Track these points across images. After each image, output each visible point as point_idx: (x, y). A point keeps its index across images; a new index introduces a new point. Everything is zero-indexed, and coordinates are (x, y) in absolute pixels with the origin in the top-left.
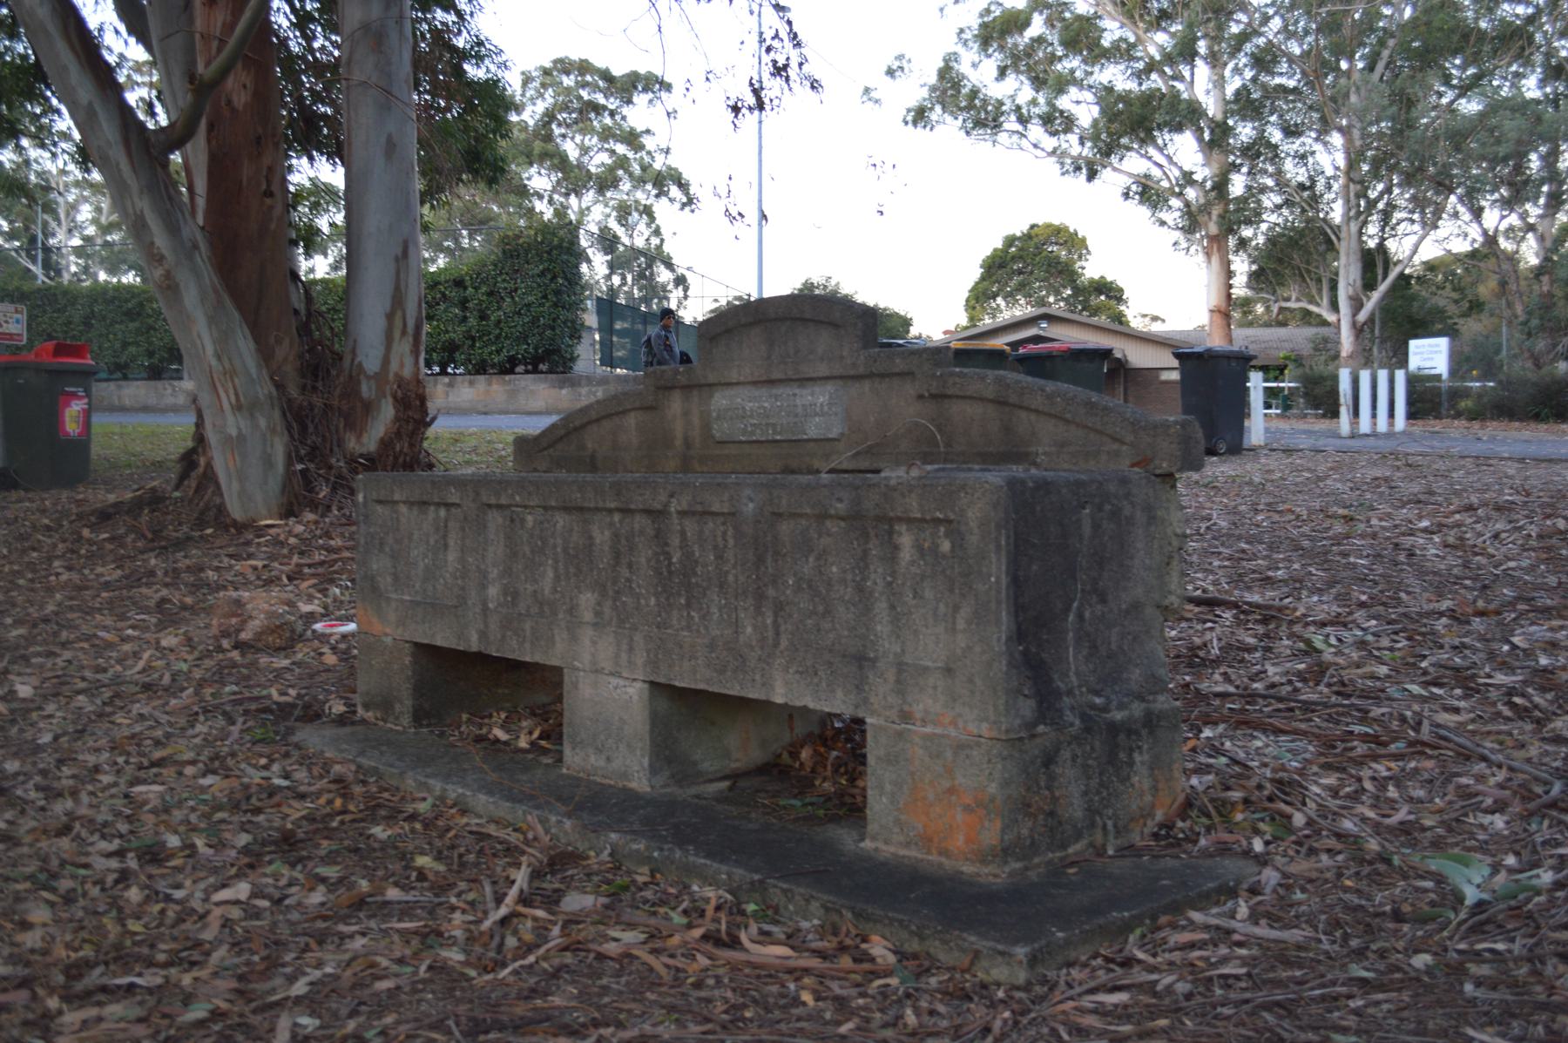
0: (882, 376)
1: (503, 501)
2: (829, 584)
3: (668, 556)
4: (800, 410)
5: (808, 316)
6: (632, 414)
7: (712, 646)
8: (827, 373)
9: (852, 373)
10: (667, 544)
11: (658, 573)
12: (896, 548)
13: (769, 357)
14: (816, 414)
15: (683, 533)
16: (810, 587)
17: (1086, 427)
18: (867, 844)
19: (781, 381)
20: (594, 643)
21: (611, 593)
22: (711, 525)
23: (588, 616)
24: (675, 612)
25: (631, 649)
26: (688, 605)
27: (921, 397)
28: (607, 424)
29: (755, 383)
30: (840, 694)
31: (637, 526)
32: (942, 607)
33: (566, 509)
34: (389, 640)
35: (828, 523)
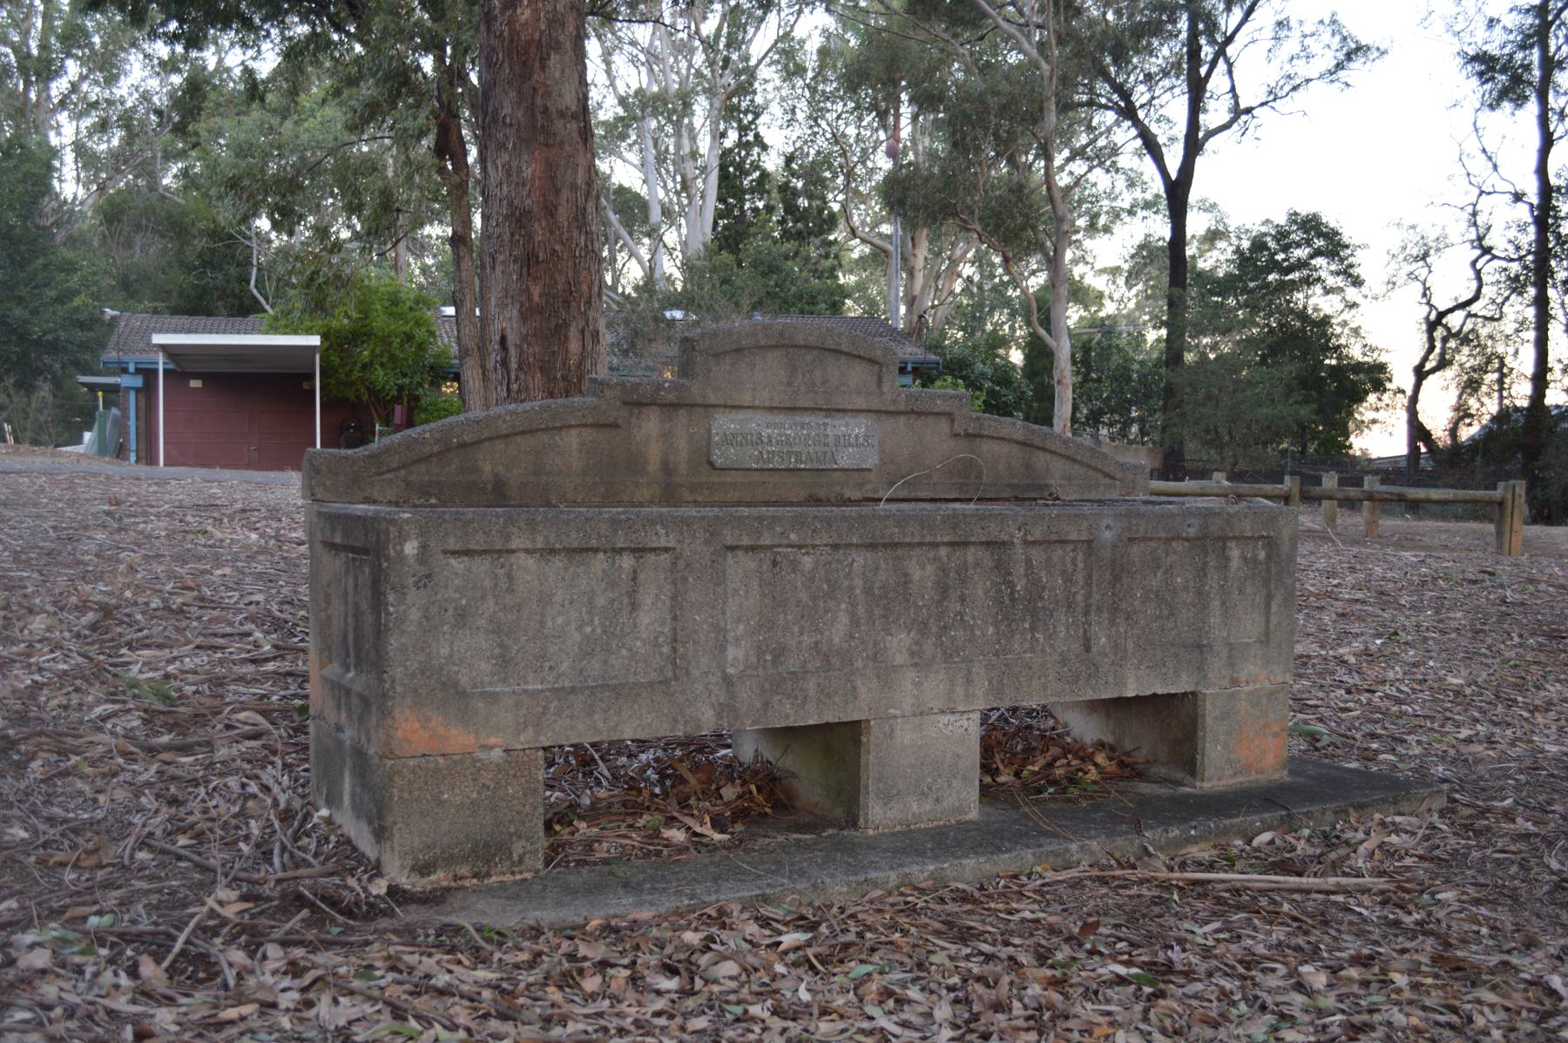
0: (920, 414)
1: (766, 540)
2: (1174, 592)
3: (1011, 585)
4: (831, 440)
5: (844, 349)
6: (574, 432)
7: (1064, 660)
8: (864, 407)
9: (892, 408)
10: (1009, 574)
11: (999, 602)
12: (1228, 559)
13: (790, 384)
14: (850, 445)
15: (1028, 561)
16: (1157, 596)
17: (1089, 466)
18: (1206, 785)
19: (806, 409)
20: (918, 685)
21: (934, 630)
22: (1060, 552)
23: (900, 659)
24: (1017, 637)
25: (969, 681)
26: (1033, 629)
27: (957, 435)
28: (525, 442)
29: (771, 409)
30: (1184, 676)
31: (970, 559)
32: (1257, 599)
33: (872, 546)
34: (497, 754)
35: (1174, 544)
